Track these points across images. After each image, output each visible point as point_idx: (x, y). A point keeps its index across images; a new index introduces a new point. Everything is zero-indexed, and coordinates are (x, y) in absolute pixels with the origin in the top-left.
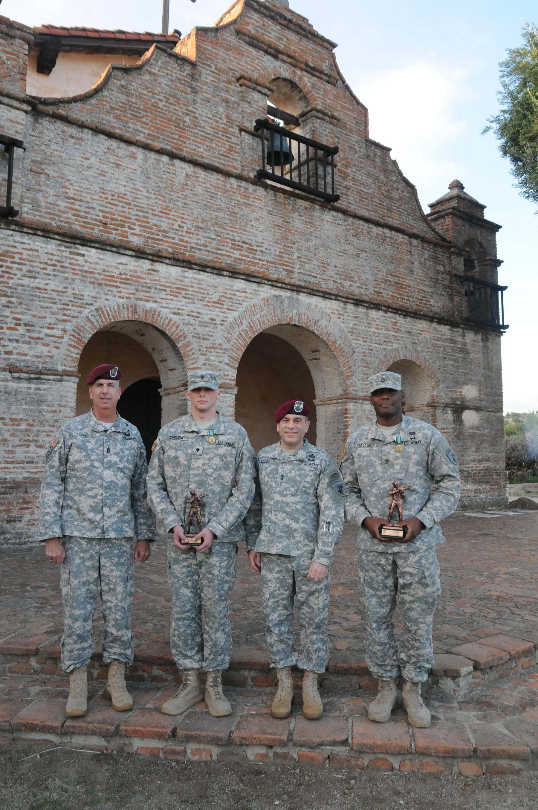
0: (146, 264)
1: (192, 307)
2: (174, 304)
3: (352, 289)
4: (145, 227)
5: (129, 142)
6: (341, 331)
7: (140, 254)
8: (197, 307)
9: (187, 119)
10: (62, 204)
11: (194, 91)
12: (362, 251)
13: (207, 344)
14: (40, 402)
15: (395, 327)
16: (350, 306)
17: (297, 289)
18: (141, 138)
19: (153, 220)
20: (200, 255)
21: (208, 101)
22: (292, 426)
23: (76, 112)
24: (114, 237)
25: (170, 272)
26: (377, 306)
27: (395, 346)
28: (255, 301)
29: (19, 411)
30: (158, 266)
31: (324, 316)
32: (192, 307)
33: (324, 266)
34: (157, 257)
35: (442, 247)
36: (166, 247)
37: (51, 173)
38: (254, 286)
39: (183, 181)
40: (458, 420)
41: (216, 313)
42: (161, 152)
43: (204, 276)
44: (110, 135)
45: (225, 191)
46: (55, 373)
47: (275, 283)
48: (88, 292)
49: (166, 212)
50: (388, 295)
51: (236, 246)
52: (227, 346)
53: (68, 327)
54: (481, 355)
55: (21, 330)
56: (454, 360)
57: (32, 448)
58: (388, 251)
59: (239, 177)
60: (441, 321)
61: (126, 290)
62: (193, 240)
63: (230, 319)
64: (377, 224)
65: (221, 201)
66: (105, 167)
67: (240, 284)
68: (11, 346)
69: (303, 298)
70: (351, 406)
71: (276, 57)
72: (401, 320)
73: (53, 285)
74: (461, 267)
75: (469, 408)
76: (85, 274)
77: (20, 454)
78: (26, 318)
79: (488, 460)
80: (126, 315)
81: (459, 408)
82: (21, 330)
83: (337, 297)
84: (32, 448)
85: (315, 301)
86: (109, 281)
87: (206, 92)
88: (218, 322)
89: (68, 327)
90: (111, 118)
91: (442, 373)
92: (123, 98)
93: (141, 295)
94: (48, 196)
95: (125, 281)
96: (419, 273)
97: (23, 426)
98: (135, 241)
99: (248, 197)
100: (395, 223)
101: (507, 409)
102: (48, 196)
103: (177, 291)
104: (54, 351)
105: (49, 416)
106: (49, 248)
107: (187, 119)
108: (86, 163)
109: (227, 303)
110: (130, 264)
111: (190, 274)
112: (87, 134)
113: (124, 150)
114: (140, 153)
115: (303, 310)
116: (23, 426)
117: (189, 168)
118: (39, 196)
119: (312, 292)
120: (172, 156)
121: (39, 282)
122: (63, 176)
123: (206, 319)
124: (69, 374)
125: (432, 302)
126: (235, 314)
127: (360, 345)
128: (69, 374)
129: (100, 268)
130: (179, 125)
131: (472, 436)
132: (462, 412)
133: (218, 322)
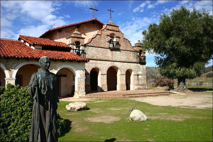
5: (94, 47)
7: (96, 60)
8: (102, 65)
17: (114, 61)
18: (95, 46)
20: (102, 59)
22: (54, 17)
23: (88, 45)
24: (93, 58)
25: (99, 62)
26: (125, 62)
31: (117, 64)
35: (135, 52)
36: (98, 59)
40: (138, 77)
42: (97, 47)
43: (103, 61)
44: (92, 47)
47: (111, 61)
48: (91, 65)
58: (127, 54)
59: (107, 48)
60: (135, 63)
62: (101, 57)
64: (125, 50)
67: (107, 62)
72: (129, 63)
74: (139, 54)
80: (94, 67)
81: (138, 75)
83: (119, 62)
96: (132, 56)
98: (95, 58)
100: (128, 50)
101: (61, 77)
103: (100, 63)
109: (105, 64)
112: (90, 47)
113: (94, 48)
114: (95, 48)
117: (101, 48)
119: (116, 61)
120: (99, 47)
124: (105, 74)
125: (134, 60)
127: (123, 68)
128: (105, 74)
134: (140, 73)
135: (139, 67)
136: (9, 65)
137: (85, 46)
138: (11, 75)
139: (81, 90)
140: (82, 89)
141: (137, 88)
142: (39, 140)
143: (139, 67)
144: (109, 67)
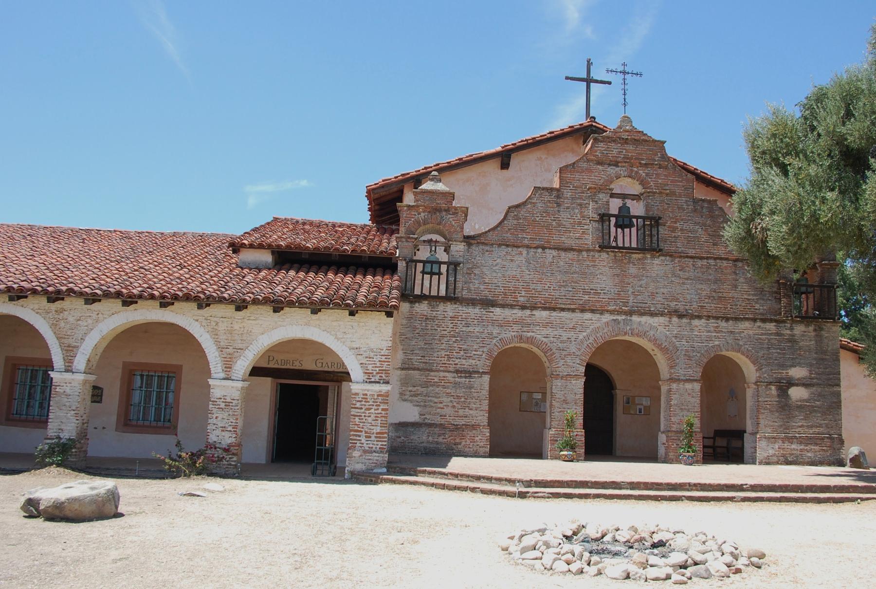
0: (528, 312)
1: (556, 333)
2: (545, 332)
3: (677, 307)
4: (528, 290)
6: (667, 337)
9: (554, 223)
10: (482, 287)
11: (559, 205)
12: (687, 279)
13: (564, 353)
14: (471, 388)
15: (717, 330)
16: (675, 319)
19: (532, 286)
21: (568, 208)
27: (717, 343)
28: (598, 325)
29: (460, 392)
30: (534, 312)
32: (556, 333)
33: (653, 295)
34: (533, 308)
37: (477, 272)
38: (598, 316)
39: (551, 260)
41: (572, 334)
43: (563, 314)
45: (578, 261)
46: (478, 372)
48: (496, 331)
49: (540, 281)
50: (711, 306)
51: (585, 293)
52: (579, 353)
53: (485, 350)
54: (813, 342)
55: (462, 353)
56: (780, 349)
57: (467, 410)
61: (516, 328)
63: (581, 337)
64: (701, 258)
65: (576, 267)
66: (505, 263)
68: (457, 361)
69: (635, 318)
70: (674, 386)
71: (617, 166)
72: (723, 324)
73: (477, 329)
75: (797, 385)
76: (493, 322)
77: (461, 412)
78: (464, 347)
79: (820, 426)
82: (462, 353)
84: (467, 410)
85: (644, 319)
86: (504, 324)
87: (567, 203)
88: (573, 340)
89: (485, 350)
90: (509, 235)
91: (766, 360)
92: (515, 222)
93: (525, 329)
94: (475, 285)
95: (516, 323)
97: (463, 400)
99: (594, 261)
102: (475, 285)
103: (548, 324)
104: (478, 362)
105: (475, 394)
106: (475, 311)
107: (554, 223)
108: (495, 263)
110: (518, 313)
111: (554, 314)
115: (635, 326)
116: (463, 400)
117: (554, 253)
118: (471, 285)
121: (470, 329)
122: (483, 273)
123: (565, 338)
126: (585, 334)
129: (501, 318)
130: (548, 227)
131: (800, 407)
132: (788, 388)
133: (573, 340)
134: (798, 372)
135: (789, 341)
136: (67, 323)
137: (469, 240)
138: (71, 362)
139: (363, 439)
140: (373, 438)
141: (771, 452)
142: (874, 485)
143: (789, 341)
144: (601, 341)
